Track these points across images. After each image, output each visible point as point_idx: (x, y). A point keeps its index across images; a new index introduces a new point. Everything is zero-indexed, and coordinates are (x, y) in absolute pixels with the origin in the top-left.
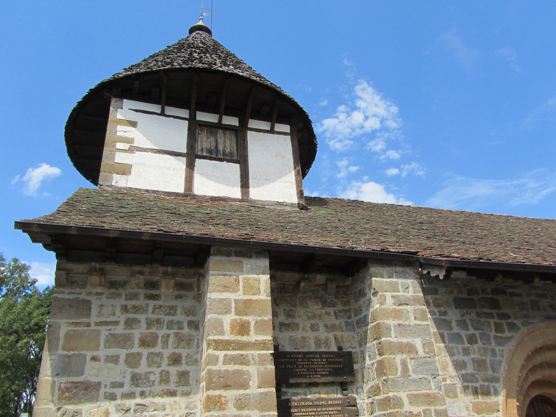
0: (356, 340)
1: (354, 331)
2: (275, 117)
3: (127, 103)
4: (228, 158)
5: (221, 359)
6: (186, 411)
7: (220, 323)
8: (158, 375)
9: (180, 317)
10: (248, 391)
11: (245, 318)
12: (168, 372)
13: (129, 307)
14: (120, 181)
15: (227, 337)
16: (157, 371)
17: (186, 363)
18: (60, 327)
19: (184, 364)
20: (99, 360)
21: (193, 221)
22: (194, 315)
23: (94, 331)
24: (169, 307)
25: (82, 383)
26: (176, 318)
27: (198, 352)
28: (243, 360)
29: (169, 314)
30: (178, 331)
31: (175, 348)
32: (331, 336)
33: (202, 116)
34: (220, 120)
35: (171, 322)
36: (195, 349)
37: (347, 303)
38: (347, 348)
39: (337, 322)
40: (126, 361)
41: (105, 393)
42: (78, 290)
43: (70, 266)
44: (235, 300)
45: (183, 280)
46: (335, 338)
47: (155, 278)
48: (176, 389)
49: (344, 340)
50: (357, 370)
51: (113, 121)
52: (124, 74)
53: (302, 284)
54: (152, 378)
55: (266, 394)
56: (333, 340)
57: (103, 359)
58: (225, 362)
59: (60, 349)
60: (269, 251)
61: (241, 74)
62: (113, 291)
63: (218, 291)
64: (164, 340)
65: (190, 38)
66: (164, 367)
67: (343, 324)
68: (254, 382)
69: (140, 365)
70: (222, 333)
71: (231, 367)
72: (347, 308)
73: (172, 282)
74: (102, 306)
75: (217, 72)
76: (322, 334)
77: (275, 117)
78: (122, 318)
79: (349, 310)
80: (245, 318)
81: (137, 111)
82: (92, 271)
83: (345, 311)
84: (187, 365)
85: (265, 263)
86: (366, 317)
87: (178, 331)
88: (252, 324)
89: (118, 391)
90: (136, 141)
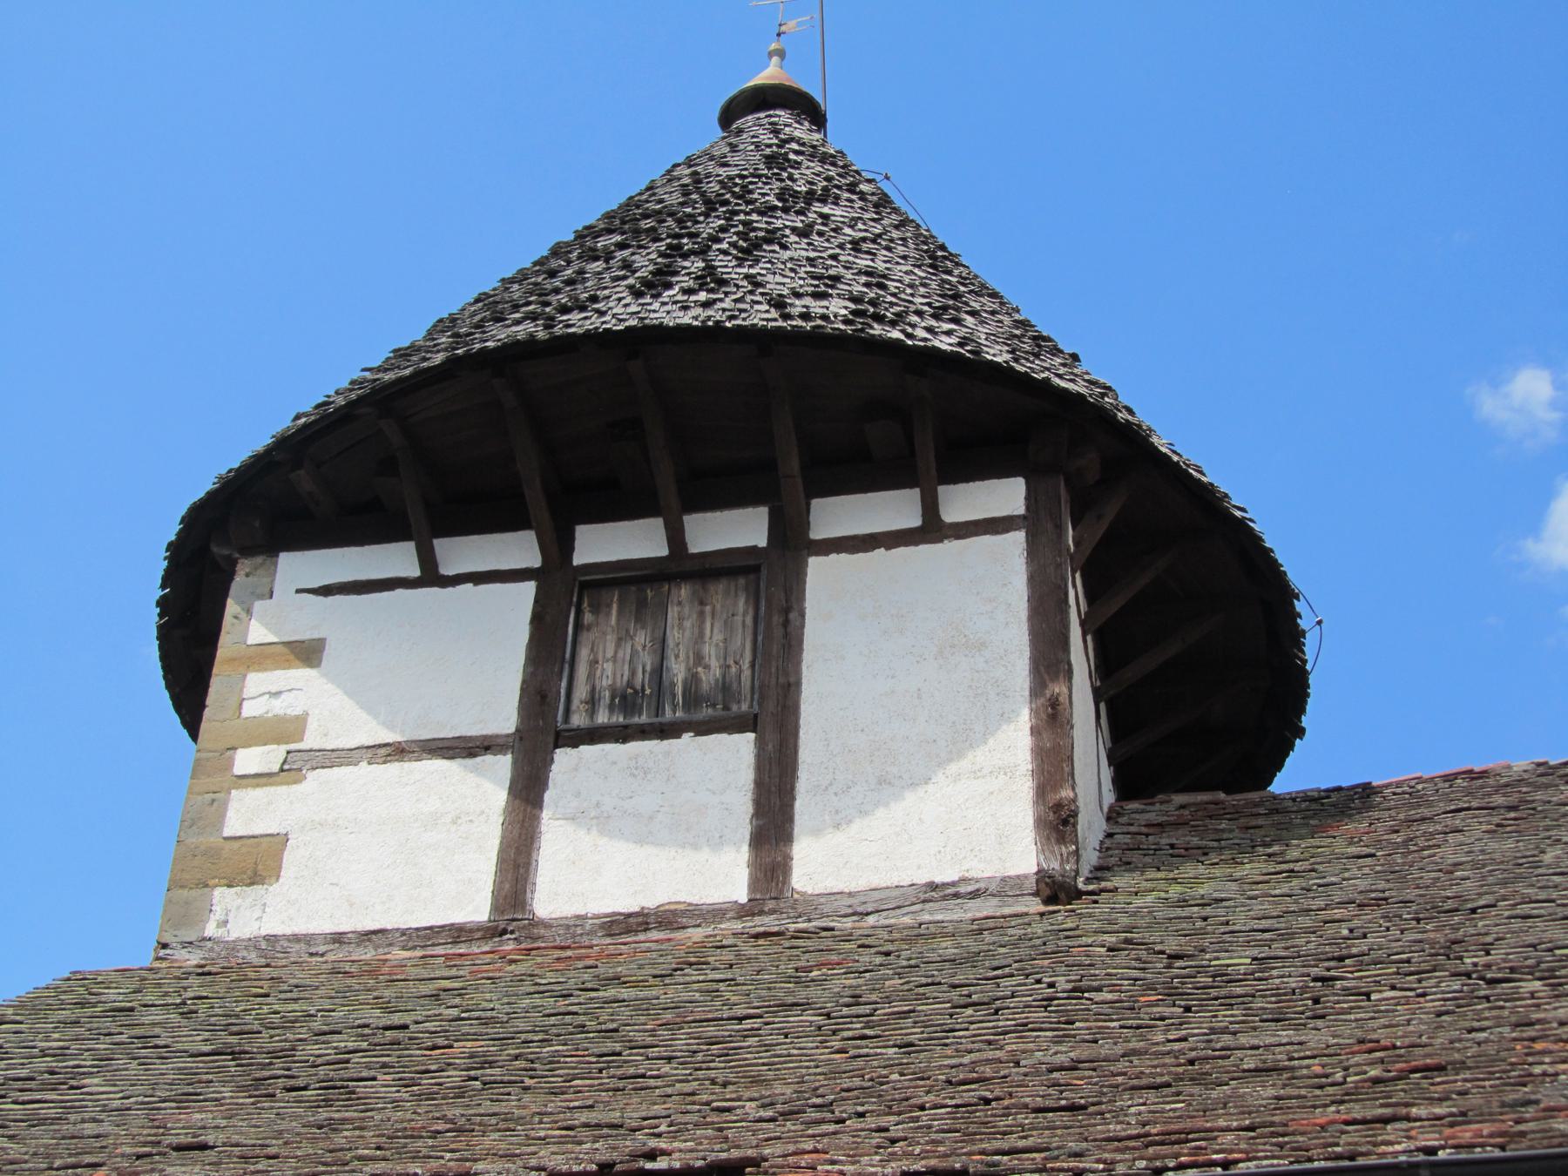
77: (927, 459)
81: (326, 591)
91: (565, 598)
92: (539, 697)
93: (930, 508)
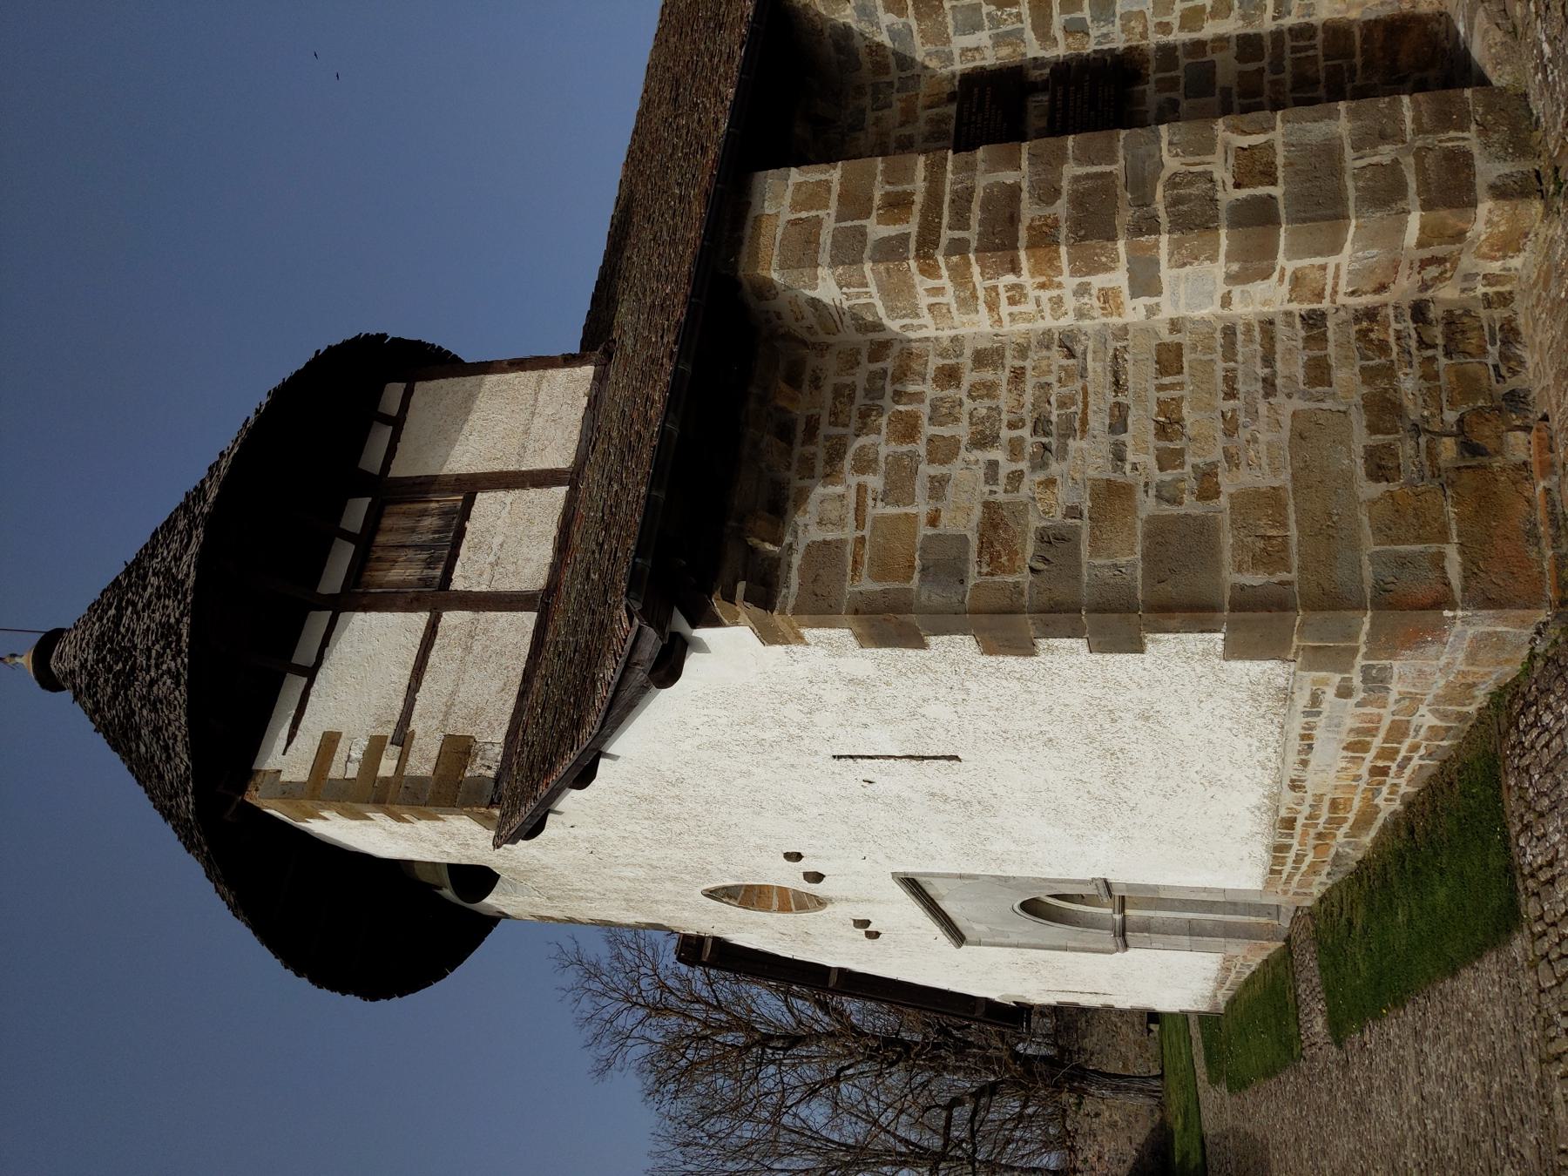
6: (1055, 348)
9: (860, 378)
10: (1025, 185)
11: (877, 201)
15: (912, 227)
16: (968, 404)
19: (960, 360)
22: (859, 352)
23: (874, 528)
29: (851, 399)
31: (924, 380)
33: (333, 579)
34: (348, 536)
37: (860, 90)
40: (943, 463)
44: (837, 221)
55: (1032, 156)
63: (817, 252)
71: (976, 214)
72: (869, 90)
79: (876, 86)
80: (877, 201)
81: (289, 743)
84: (961, 355)
86: (895, 53)
89: (1006, 468)
90: (380, 732)
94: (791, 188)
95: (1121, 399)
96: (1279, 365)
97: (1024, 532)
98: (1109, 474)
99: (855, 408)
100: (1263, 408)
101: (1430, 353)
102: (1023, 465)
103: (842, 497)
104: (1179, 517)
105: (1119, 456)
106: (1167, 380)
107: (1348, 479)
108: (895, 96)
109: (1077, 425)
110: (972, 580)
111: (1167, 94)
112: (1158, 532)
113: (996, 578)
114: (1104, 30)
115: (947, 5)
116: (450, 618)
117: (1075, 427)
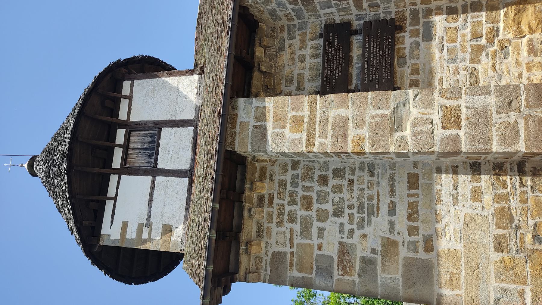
0: (314, 20)
1: (307, 22)
2: (116, 95)
3: (105, 230)
4: (156, 139)
5: (322, 140)
7: (293, 141)
8: (335, 195)
11: (289, 118)
12: (333, 186)
13: (278, 220)
14: (178, 234)
16: (332, 195)
17: (326, 171)
18: (294, 277)
19: (328, 173)
20: (322, 243)
21: (209, 168)
24: (279, 186)
25: (339, 257)
26: (289, 180)
27: (318, 161)
28: (324, 122)
30: (300, 178)
31: (314, 181)
32: (310, 44)
33: (117, 163)
35: (292, 184)
36: (315, 163)
38: (319, 30)
39: (298, 38)
41: (348, 238)
42: (263, 263)
43: (242, 271)
45: (257, 174)
46: (312, 40)
47: (255, 198)
48: (347, 180)
49: (314, 31)
50: (340, 21)
51: (122, 242)
52: (76, 234)
53: (263, 69)
54: (337, 199)
56: (314, 42)
57: (321, 241)
58: (325, 137)
59: (311, 276)
60: (231, 98)
61: (72, 126)
62: (264, 234)
64: (306, 190)
65: (41, 175)
66: (329, 190)
67: (300, 32)
68: (343, 112)
69: (326, 210)
70: (301, 139)
71: (330, 131)
72: (286, 28)
73: (258, 184)
74: (277, 243)
75: (70, 149)
76: (308, 52)
77: (116, 95)
78: (287, 225)
81: (112, 222)
82: (247, 252)
83: (289, 30)
85: (241, 101)
87: (300, 178)
88: (294, 113)
89: (347, 227)
91: (126, 169)
92: (144, 172)
93: (126, 97)
94: (254, 109)
95: (393, 199)
96: (460, 190)
97: (355, 258)
98: (388, 235)
99: (287, 191)
100: (452, 209)
101: (524, 189)
102: (354, 227)
103: (284, 233)
104: (416, 259)
105: (392, 224)
106: (413, 192)
107: (486, 250)
108: (297, 33)
109: (375, 210)
110: (336, 277)
111: (414, 39)
112: (409, 264)
113: (345, 277)
114: (387, 6)
115: (316, 1)
116: (159, 179)
117: (373, 211)
